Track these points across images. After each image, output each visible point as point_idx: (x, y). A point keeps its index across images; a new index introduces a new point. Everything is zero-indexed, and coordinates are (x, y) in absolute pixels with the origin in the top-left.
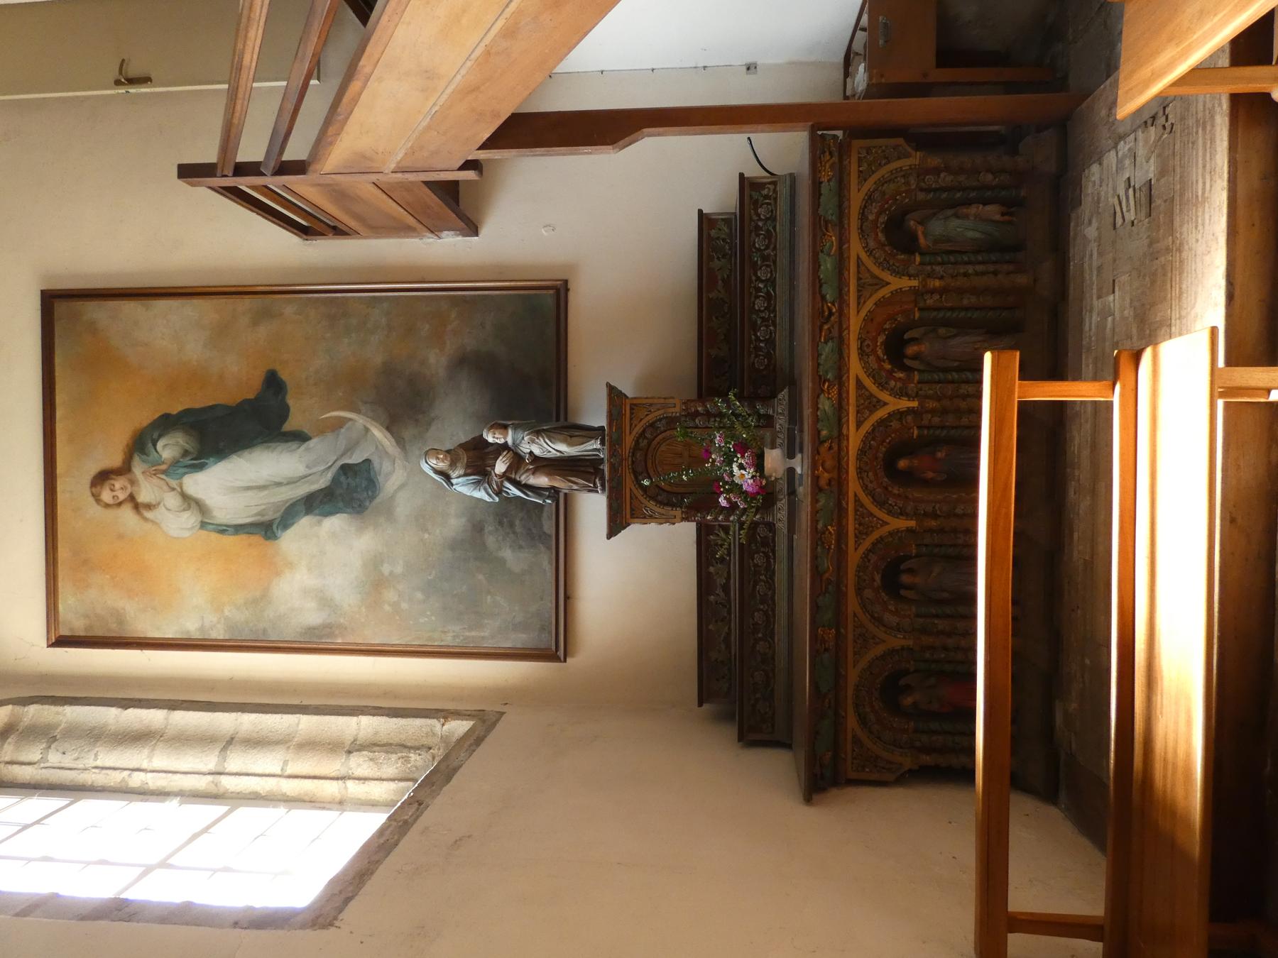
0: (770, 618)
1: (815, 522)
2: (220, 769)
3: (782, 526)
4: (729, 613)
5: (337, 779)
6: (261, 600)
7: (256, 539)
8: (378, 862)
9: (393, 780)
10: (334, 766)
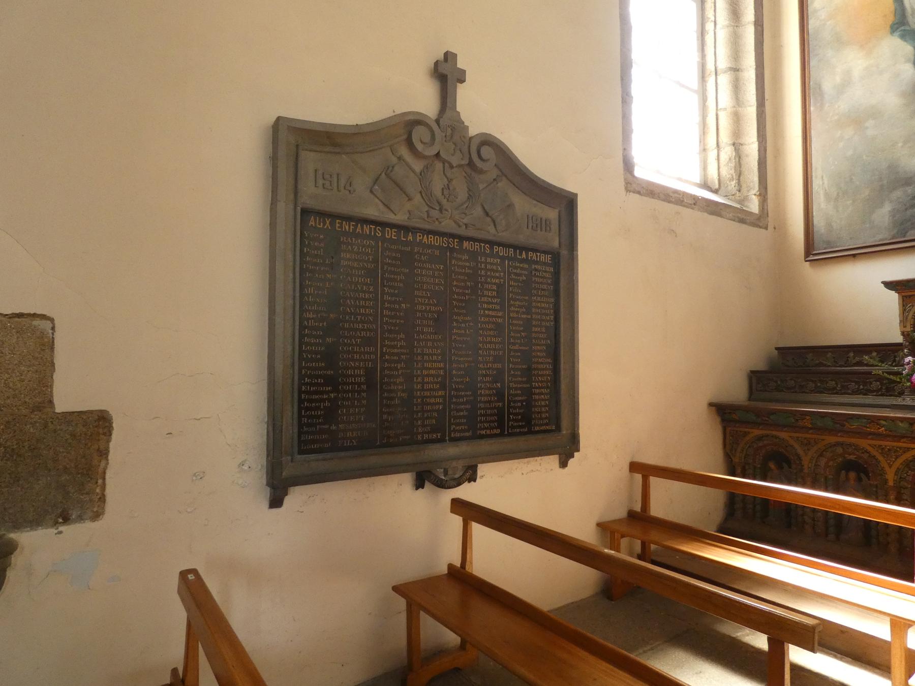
0: (833, 391)
1: (886, 419)
2: (719, 72)
3: (899, 401)
4: (841, 366)
5: (718, 144)
6: (839, 42)
7: (891, 19)
8: (659, 198)
9: (719, 175)
10: (725, 138)
